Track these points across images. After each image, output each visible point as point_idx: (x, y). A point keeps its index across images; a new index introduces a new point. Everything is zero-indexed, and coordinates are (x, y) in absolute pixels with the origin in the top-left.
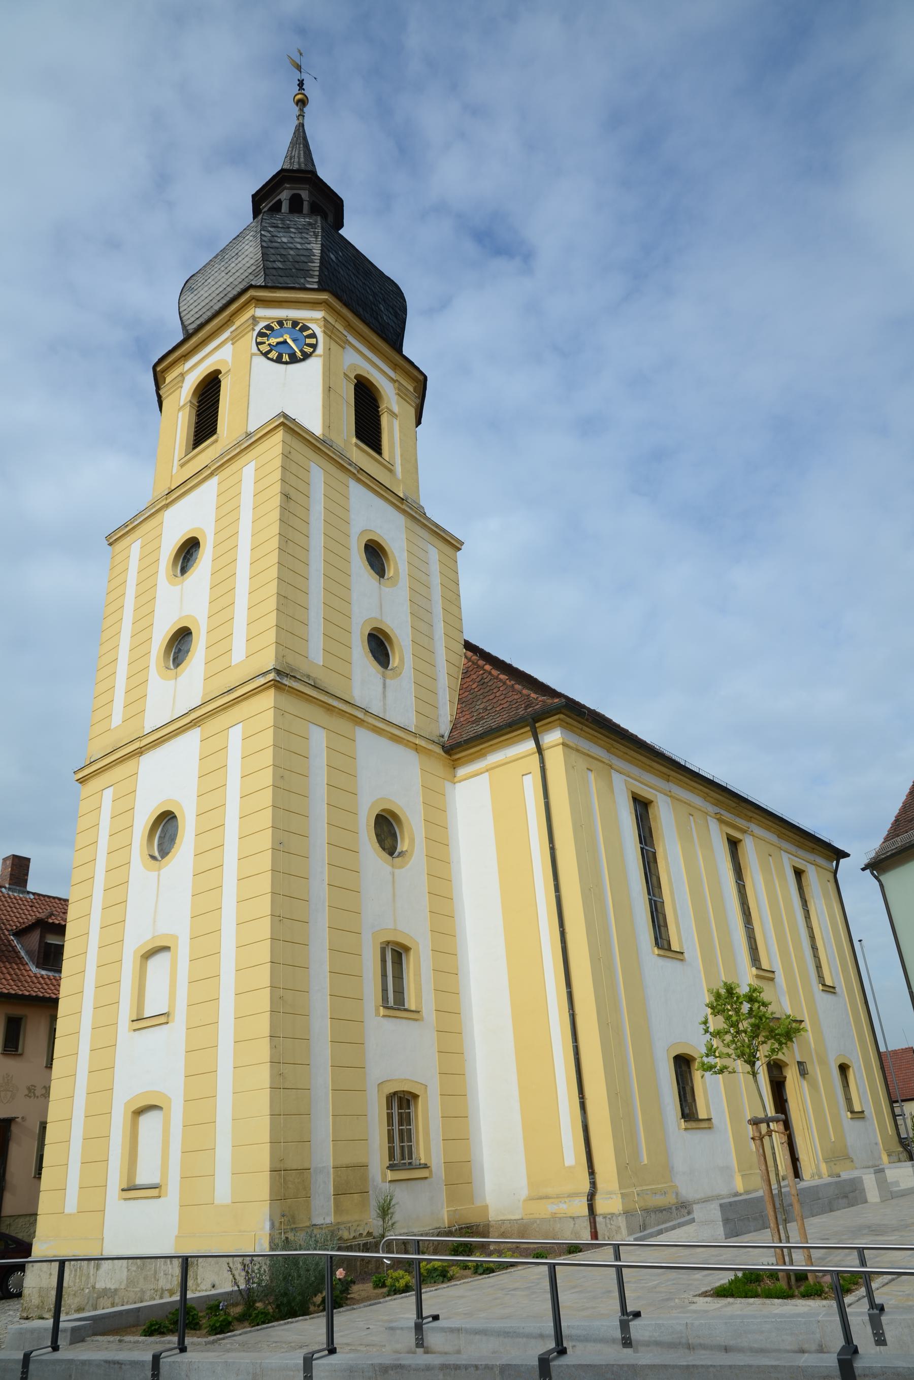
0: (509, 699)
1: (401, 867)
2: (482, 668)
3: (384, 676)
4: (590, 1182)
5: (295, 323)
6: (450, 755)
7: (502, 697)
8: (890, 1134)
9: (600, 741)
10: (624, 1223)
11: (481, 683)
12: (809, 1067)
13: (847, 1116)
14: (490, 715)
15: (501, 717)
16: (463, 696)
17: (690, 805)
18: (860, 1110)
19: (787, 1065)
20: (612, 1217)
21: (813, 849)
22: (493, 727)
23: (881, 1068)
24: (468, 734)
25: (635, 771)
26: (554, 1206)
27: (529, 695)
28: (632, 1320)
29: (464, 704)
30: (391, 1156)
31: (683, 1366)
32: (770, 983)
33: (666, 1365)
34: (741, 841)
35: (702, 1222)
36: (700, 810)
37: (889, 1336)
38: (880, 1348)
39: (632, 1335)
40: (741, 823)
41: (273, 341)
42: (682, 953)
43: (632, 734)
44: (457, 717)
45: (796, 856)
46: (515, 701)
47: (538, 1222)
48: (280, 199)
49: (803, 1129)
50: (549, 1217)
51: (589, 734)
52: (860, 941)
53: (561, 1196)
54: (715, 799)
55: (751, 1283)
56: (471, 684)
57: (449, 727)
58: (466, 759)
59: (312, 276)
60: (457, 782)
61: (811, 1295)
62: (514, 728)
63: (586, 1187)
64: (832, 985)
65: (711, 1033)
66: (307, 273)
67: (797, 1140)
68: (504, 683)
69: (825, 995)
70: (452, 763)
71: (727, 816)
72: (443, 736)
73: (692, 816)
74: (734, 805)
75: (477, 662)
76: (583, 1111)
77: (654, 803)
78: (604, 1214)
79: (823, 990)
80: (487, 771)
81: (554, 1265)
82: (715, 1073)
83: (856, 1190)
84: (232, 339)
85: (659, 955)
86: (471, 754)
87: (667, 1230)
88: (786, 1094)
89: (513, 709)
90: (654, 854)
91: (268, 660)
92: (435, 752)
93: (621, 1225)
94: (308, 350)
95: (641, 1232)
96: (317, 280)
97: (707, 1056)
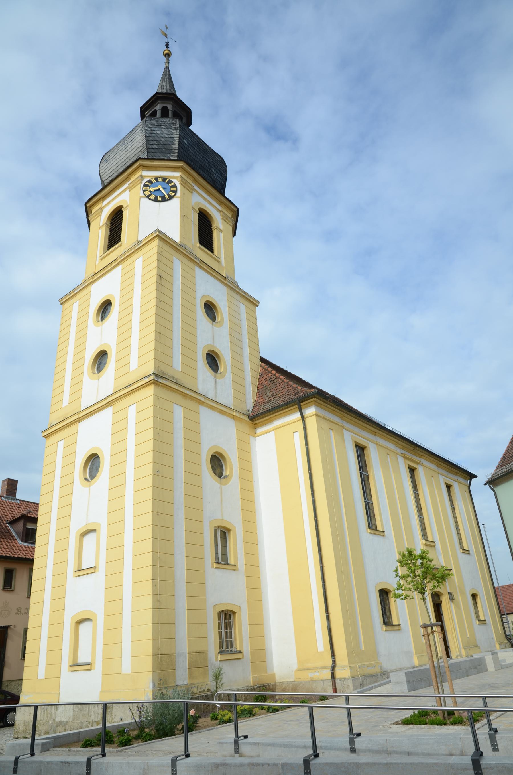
0: (286, 390)
1: (226, 484)
2: (271, 372)
3: (215, 377)
4: (332, 660)
5: (164, 179)
6: (253, 421)
7: (282, 388)
8: (501, 632)
9: (336, 413)
10: (352, 683)
11: (270, 380)
12: (455, 596)
13: (476, 622)
15: (281, 400)
16: (260, 388)
17: (387, 449)
19: (442, 594)
20: (345, 680)
22: (277, 405)
25: (356, 430)
26: (312, 674)
28: (355, 738)
29: (261, 393)
30: (221, 646)
32: (433, 548)
34: (416, 469)
36: (393, 452)
38: (495, 753)
40: (417, 459)
41: (152, 189)
42: (383, 532)
44: (257, 400)
45: (447, 477)
46: (289, 391)
47: (303, 683)
48: (156, 110)
49: (452, 630)
50: (309, 680)
52: (483, 525)
56: (264, 381)
57: (252, 405)
59: (174, 153)
60: (256, 436)
61: (456, 723)
63: (330, 663)
64: (467, 550)
66: (171, 151)
67: (448, 637)
71: (408, 455)
72: (248, 411)
73: (389, 455)
74: (412, 449)
76: (328, 621)
77: (367, 448)
78: (340, 678)
79: (462, 552)
80: (274, 430)
81: (312, 707)
82: (402, 599)
83: (481, 664)
84: (129, 189)
85: (370, 533)
86: (265, 421)
89: (288, 395)
90: (368, 476)
91: (150, 368)
92: (244, 420)
93: (350, 684)
94: (172, 194)
96: (177, 155)
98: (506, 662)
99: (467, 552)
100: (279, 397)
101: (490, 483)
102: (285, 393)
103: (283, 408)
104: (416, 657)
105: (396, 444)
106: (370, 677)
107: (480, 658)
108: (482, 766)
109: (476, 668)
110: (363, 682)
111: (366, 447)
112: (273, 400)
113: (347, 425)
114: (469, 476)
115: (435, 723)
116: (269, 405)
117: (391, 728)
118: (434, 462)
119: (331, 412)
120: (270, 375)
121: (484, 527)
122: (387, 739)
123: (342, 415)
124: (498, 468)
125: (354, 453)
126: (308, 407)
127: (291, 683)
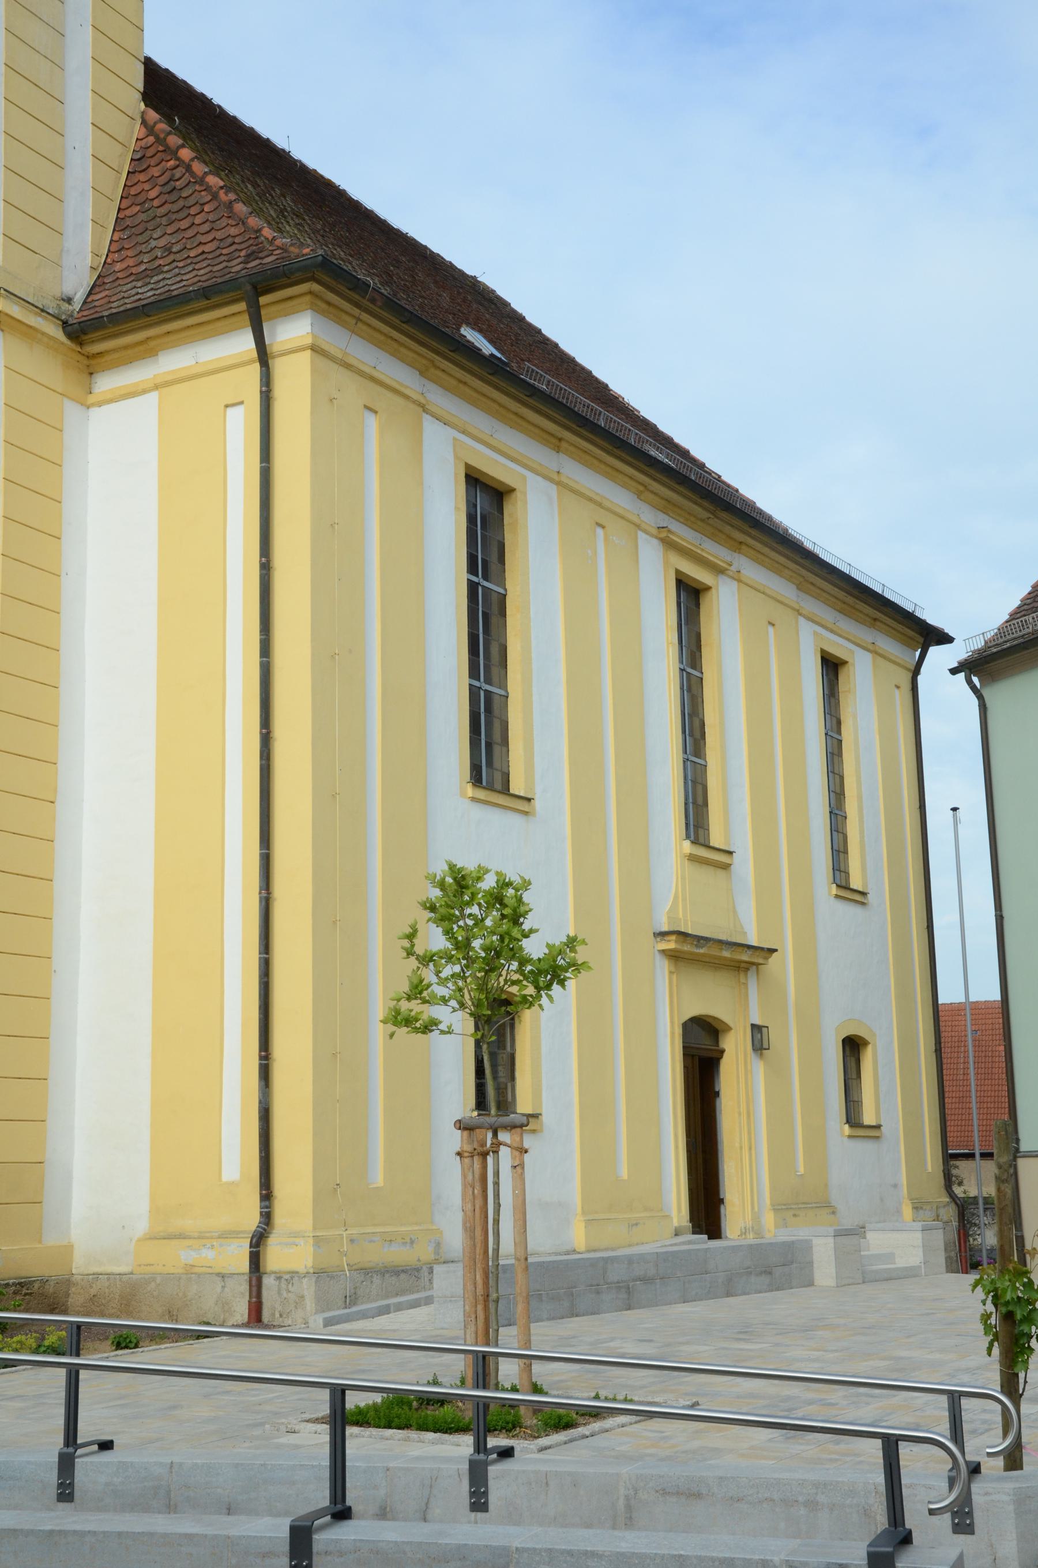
0: (219, 235)
2: (174, 153)
4: (261, 1213)
6: (81, 344)
7: (206, 227)
8: (930, 1169)
9: (403, 350)
10: (313, 1289)
11: (168, 188)
12: (774, 1036)
13: (842, 1130)
14: (175, 264)
15: (195, 273)
16: (128, 213)
17: (600, 505)
18: (874, 1124)
19: (728, 1028)
20: (292, 1278)
21: (875, 620)
22: (175, 293)
23: (936, 1050)
24: (122, 302)
25: (481, 422)
26: (192, 1253)
27: (259, 231)
28: (494, 1462)
29: (127, 232)
31: (43, 1531)
32: (721, 873)
33: (15, 1530)
34: (708, 588)
35: (448, 1297)
36: (622, 517)
37: (494, 1498)
38: (476, 1516)
39: (76, 1481)
40: (714, 550)
42: (529, 800)
43: (548, 339)
44: (109, 260)
45: (832, 631)
46: (230, 240)
47: (158, 1281)
49: (741, 1148)
50: (181, 1271)
51: (381, 332)
52: (954, 809)
53: (208, 1235)
54: (662, 498)
55: (428, 1404)
56: (147, 187)
57: (87, 280)
58: (116, 356)
60: (93, 405)
61: (495, 1430)
62: (215, 300)
63: (252, 1220)
64: (860, 889)
65: (418, 955)
67: (725, 1167)
68: (215, 197)
69: (842, 907)
70: (86, 362)
71: (684, 534)
72: (69, 300)
73: (603, 527)
74: (705, 515)
75: (165, 139)
76: (263, 1083)
77: (518, 494)
78: (280, 1272)
79: (837, 896)
80: (156, 387)
82: (417, 1030)
83: (792, 1263)
85: (473, 799)
86: (126, 347)
87: (399, 1307)
88: (719, 1083)
89: (222, 258)
90: (503, 597)
92: (43, 334)
93: (306, 1293)
95: (346, 1308)
97: (409, 998)
98: (895, 1263)
99: (858, 897)
100: (189, 261)
101: (970, 670)
102: (215, 244)
103: (196, 305)
104: (583, 1225)
105: (641, 492)
106: (387, 1276)
107: (793, 1242)
108: (316, 1548)
109: (770, 1273)
110: (355, 1288)
111: (511, 490)
112: (166, 268)
113: (439, 399)
114: (921, 634)
115: (431, 1427)
116: (150, 287)
117: (294, 1432)
118: (786, 571)
119: (379, 345)
120: (172, 163)
121: (955, 817)
122: (172, 1463)
123: (424, 362)
124: (1014, 615)
125: (457, 508)
126: (287, 314)
127: (120, 1280)
